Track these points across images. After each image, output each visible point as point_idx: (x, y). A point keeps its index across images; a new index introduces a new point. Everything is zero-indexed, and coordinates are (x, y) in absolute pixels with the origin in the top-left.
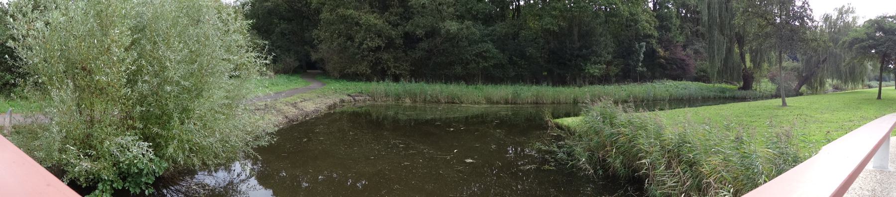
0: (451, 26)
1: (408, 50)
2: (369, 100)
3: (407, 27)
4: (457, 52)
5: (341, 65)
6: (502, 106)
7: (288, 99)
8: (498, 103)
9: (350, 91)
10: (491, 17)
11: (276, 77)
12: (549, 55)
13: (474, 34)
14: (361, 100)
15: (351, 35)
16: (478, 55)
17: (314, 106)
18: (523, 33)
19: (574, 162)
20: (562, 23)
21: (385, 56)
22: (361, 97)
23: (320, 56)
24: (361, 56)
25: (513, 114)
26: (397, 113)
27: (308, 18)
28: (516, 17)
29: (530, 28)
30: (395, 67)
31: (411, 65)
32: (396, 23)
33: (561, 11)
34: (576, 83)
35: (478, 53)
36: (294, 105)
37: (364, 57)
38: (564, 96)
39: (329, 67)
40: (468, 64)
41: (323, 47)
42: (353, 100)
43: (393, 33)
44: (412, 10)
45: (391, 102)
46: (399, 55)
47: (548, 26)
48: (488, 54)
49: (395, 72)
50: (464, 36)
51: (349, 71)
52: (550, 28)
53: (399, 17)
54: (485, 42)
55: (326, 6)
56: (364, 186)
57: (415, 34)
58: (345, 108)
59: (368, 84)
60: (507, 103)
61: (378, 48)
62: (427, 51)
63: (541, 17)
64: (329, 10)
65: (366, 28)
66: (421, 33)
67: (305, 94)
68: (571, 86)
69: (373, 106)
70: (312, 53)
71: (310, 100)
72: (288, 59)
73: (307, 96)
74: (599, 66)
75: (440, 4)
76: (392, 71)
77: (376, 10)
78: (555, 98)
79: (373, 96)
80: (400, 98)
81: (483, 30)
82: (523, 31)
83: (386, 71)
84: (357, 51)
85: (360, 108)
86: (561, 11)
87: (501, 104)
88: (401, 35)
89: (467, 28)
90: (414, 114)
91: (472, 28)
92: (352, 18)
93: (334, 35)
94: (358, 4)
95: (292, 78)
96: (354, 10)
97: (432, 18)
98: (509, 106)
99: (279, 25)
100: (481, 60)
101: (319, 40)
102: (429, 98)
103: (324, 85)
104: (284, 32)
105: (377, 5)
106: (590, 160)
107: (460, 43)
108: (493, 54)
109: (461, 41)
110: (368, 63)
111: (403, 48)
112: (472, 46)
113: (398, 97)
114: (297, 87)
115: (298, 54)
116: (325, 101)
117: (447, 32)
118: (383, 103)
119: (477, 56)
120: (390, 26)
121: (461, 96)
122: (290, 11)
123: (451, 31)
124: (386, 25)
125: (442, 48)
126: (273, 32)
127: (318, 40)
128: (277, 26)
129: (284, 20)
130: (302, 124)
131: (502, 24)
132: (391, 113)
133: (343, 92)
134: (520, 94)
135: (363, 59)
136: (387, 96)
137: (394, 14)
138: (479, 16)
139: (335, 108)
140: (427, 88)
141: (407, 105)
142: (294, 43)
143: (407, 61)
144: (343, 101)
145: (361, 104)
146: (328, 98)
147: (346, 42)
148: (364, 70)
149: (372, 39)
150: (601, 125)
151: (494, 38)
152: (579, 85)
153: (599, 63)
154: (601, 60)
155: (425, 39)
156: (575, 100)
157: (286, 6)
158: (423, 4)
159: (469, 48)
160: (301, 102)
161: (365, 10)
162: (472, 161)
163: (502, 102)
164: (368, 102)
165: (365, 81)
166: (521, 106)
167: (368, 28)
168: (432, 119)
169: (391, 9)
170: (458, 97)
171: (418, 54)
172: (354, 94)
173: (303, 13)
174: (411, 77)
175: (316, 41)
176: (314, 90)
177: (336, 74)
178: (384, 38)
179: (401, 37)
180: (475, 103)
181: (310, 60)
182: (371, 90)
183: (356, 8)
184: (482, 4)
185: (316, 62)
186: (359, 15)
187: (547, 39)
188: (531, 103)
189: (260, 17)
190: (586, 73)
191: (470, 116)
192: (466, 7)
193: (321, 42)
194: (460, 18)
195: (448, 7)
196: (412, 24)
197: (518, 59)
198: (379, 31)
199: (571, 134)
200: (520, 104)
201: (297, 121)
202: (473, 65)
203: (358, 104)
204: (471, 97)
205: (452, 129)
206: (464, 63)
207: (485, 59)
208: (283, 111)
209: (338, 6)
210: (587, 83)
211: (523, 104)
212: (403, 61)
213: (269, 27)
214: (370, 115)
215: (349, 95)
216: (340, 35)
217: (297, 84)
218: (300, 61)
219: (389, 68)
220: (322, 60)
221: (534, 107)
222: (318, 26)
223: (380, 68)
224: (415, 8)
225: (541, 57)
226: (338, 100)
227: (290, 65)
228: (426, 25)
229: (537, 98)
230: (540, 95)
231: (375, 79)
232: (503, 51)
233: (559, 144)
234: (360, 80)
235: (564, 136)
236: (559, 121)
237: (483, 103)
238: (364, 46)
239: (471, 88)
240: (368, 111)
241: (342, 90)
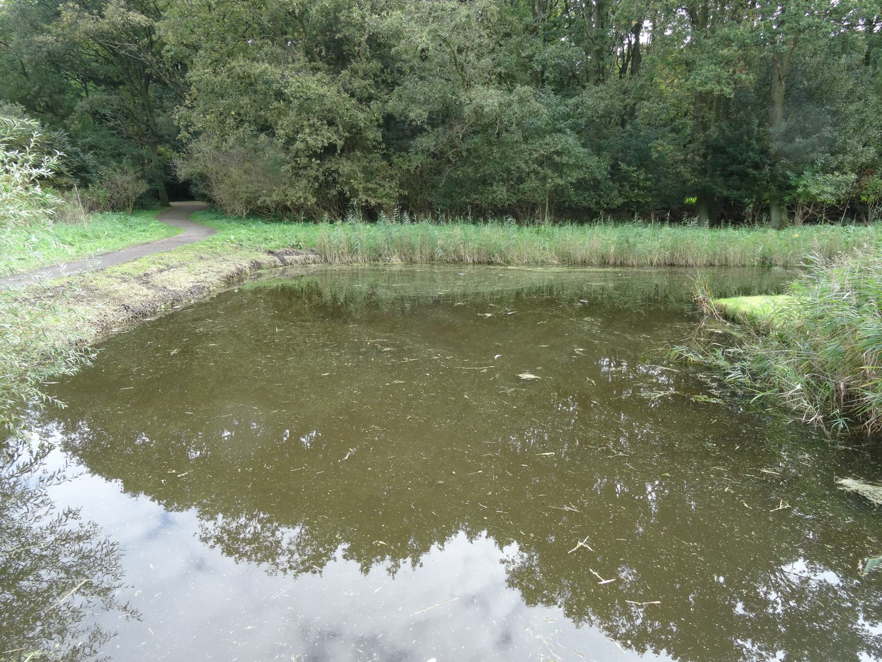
0: (485, 97)
1: (394, 153)
2: (314, 262)
3: (391, 103)
4: (498, 155)
5: (247, 187)
6: (594, 269)
7: (127, 267)
8: (584, 263)
9: (273, 244)
10: (574, 76)
11: (91, 220)
12: (705, 156)
13: (536, 114)
14: (296, 262)
15: (266, 121)
16: (547, 161)
17: (192, 278)
18: (645, 107)
19: (768, 393)
20: (744, 76)
21: (345, 166)
22: (298, 254)
23: (199, 168)
24: (293, 168)
25: (616, 288)
26: (373, 286)
27: (159, 80)
28: (628, 72)
29: (661, 97)
30: (366, 190)
31: (401, 186)
32: (366, 95)
33: (743, 46)
34: (769, 220)
35: (543, 155)
36: (145, 279)
37: (300, 169)
38: (738, 248)
39: (220, 193)
40: (521, 180)
41: (203, 147)
42: (278, 263)
43: (361, 116)
44: (398, 64)
45: (361, 264)
46: (375, 165)
47: (708, 87)
48: (565, 159)
49: (367, 201)
50: (515, 122)
51: (268, 199)
52: (712, 92)
53: (371, 81)
54: (560, 131)
55: (201, 52)
56: (316, 443)
57: (407, 117)
58: (263, 281)
59: (311, 227)
60: (604, 263)
61: (330, 149)
62: (434, 155)
63: (689, 65)
64: (209, 61)
65: (301, 105)
66: (421, 115)
67: (167, 255)
68: (757, 226)
69: (324, 274)
70: (178, 162)
71: (182, 265)
72: (117, 177)
73: (173, 257)
74: (838, 177)
75: (460, 51)
76: (360, 200)
77: (320, 64)
78: (715, 253)
79: (322, 254)
80: (380, 256)
81: (557, 106)
82: (646, 103)
83: (348, 200)
84: (282, 155)
85: (295, 278)
86: (743, 46)
87: (592, 265)
88: (377, 120)
89: (521, 101)
90: (409, 289)
91: (533, 101)
92: (266, 83)
93: (228, 121)
94: (279, 50)
95: (133, 220)
96: (270, 63)
97: (443, 81)
98: (610, 269)
99: (84, 94)
100: (549, 172)
101: (191, 130)
102: (440, 253)
103: (212, 231)
104: (102, 111)
105: (323, 53)
106: (811, 390)
107: (504, 134)
108: (577, 157)
109: (507, 131)
110: (309, 181)
111: (383, 149)
112: (530, 141)
113: (376, 255)
114: (148, 240)
115: (143, 165)
116: (217, 266)
117: (476, 113)
118: (344, 267)
119: (541, 164)
120: (353, 102)
121: (508, 248)
122: (108, 62)
123: (486, 109)
124: (344, 99)
125: (465, 146)
126: (71, 110)
127: (187, 131)
128: (78, 95)
129: (98, 82)
130: (171, 318)
131: (597, 89)
132: (362, 286)
133: (257, 245)
134: (635, 245)
135: (297, 175)
136: (352, 251)
137: (361, 73)
138: (547, 74)
139: (241, 280)
140: (436, 232)
141: (394, 268)
142: (129, 137)
143: (392, 177)
144: (257, 265)
145: (299, 271)
146: (224, 260)
147: (257, 136)
148: (300, 197)
149: (317, 130)
150: (852, 313)
151: (580, 121)
152: (778, 225)
153: (838, 168)
154: (841, 163)
155: (429, 129)
156: (764, 258)
157: (98, 47)
158: (423, 50)
159: (524, 146)
160: (161, 271)
161: (297, 65)
162: (533, 376)
163: (593, 261)
164: (313, 265)
165: (305, 220)
166: (635, 270)
167: (305, 105)
168: (447, 296)
169: (354, 64)
170: (501, 252)
171: (416, 161)
172: (282, 250)
173: (145, 67)
174: (402, 211)
175: (183, 134)
176: (188, 245)
177: (239, 208)
178: (341, 129)
179: (379, 126)
180: (537, 263)
181: (175, 178)
182: (317, 241)
183: (274, 60)
184: (554, 47)
185: (187, 183)
186: (283, 76)
187: (703, 117)
188: (658, 265)
189: (29, 70)
190: (799, 195)
191: (526, 291)
192: (519, 55)
193: (196, 134)
194: (506, 80)
195: (479, 57)
196: (401, 96)
197: (631, 169)
198: (329, 111)
199: (758, 333)
200: (633, 266)
201: (155, 313)
202: (532, 183)
203: (291, 271)
204: (529, 250)
205: (489, 315)
206: (512, 179)
207: (558, 168)
208: (116, 296)
209: (230, 54)
210: (798, 219)
211: (641, 266)
212: (384, 178)
213: (56, 97)
214: (320, 294)
215: (271, 252)
216: (242, 120)
217: (148, 234)
218: (150, 181)
219: (354, 193)
220: (203, 177)
221: (664, 273)
222: (184, 99)
223: (335, 193)
224: (404, 61)
225: (685, 161)
226: (245, 264)
227: (126, 190)
228: (430, 97)
229: (672, 254)
230: (680, 246)
231: (326, 215)
232: (598, 150)
233: (729, 353)
234: (294, 220)
235: (740, 336)
236: (730, 303)
237: (553, 264)
238: (299, 145)
239: (527, 232)
240: (313, 285)
241: (255, 242)
